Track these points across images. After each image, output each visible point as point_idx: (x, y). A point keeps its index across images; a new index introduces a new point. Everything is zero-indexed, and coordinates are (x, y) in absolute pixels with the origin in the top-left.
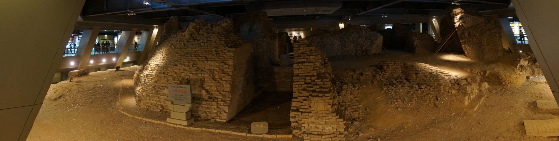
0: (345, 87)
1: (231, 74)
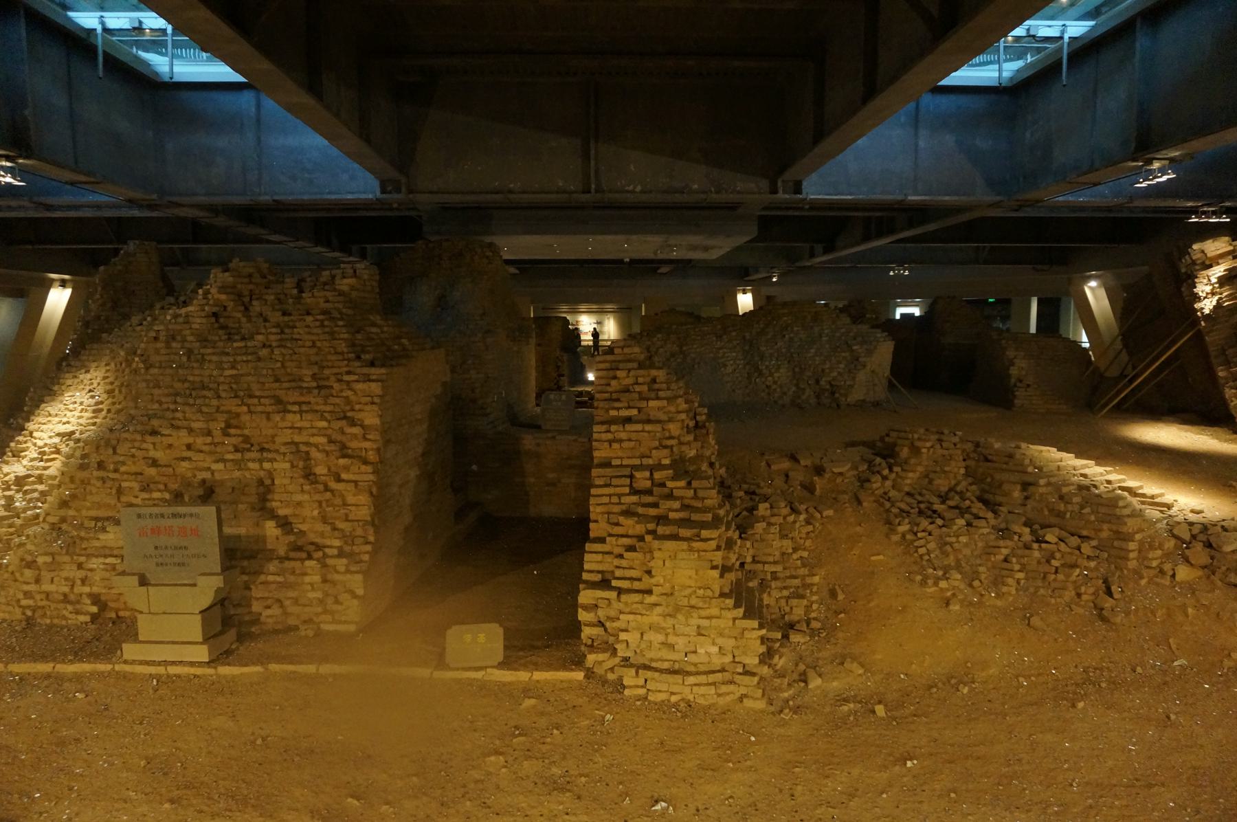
0: (763, 509)
1: (372, 456)
